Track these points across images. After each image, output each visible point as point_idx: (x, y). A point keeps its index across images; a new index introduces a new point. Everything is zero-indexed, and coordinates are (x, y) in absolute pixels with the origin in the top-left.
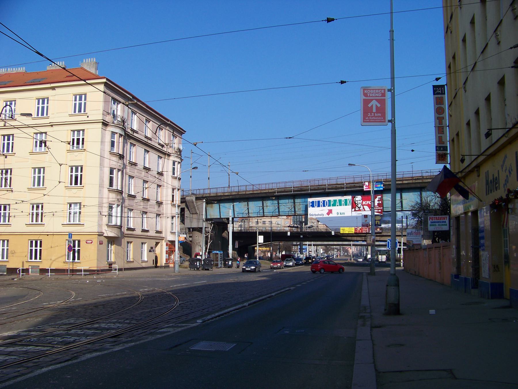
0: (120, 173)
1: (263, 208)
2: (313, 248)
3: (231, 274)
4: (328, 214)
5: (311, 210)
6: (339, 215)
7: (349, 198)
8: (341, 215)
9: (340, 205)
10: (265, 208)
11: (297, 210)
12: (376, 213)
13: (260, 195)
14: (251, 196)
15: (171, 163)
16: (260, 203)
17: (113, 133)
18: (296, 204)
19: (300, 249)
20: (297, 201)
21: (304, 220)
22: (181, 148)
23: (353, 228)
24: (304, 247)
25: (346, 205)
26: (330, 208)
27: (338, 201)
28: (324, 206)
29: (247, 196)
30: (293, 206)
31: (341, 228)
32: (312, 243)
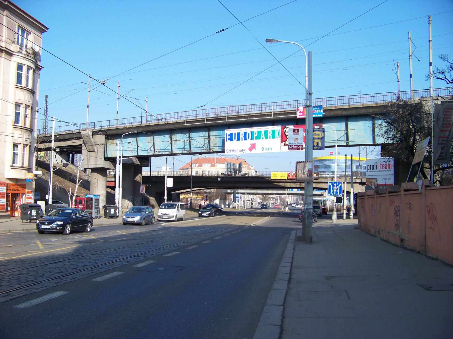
0: (29, 111)
1: (171, 144)
2: (248, 197)
3: (113, 226)
4: (250, 149)
5: (229, 145)
6: (265, 151)
7: (278, 128)
8: (267, 151)
9: (266, 138)
10: (173, 142)
11: (212, 145)
12: (316, 141)
13: (167, 127)
14: (156, 128)
15: (15, 67)
16: (167, 138)
17: (20, 67)
18: (211, 137)
19: (234, 197)
20: (213, 133)
21: (238, 168)
22: (37, 49)
23: (286, 173)
24: (237, 195)
25: (274, 137)
26: (253, 142)
27: (263, 133)
28: (245, 139)
29: (151, 129)
30: (207, 140)
31: (272, 173)
32: (246, 191)
